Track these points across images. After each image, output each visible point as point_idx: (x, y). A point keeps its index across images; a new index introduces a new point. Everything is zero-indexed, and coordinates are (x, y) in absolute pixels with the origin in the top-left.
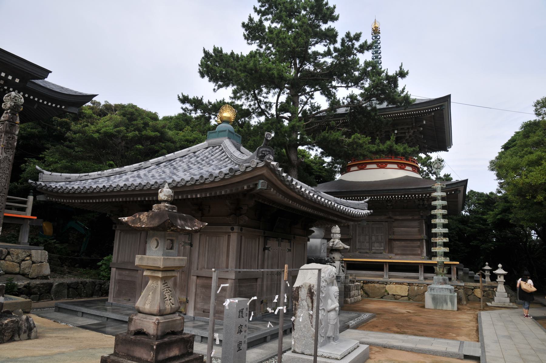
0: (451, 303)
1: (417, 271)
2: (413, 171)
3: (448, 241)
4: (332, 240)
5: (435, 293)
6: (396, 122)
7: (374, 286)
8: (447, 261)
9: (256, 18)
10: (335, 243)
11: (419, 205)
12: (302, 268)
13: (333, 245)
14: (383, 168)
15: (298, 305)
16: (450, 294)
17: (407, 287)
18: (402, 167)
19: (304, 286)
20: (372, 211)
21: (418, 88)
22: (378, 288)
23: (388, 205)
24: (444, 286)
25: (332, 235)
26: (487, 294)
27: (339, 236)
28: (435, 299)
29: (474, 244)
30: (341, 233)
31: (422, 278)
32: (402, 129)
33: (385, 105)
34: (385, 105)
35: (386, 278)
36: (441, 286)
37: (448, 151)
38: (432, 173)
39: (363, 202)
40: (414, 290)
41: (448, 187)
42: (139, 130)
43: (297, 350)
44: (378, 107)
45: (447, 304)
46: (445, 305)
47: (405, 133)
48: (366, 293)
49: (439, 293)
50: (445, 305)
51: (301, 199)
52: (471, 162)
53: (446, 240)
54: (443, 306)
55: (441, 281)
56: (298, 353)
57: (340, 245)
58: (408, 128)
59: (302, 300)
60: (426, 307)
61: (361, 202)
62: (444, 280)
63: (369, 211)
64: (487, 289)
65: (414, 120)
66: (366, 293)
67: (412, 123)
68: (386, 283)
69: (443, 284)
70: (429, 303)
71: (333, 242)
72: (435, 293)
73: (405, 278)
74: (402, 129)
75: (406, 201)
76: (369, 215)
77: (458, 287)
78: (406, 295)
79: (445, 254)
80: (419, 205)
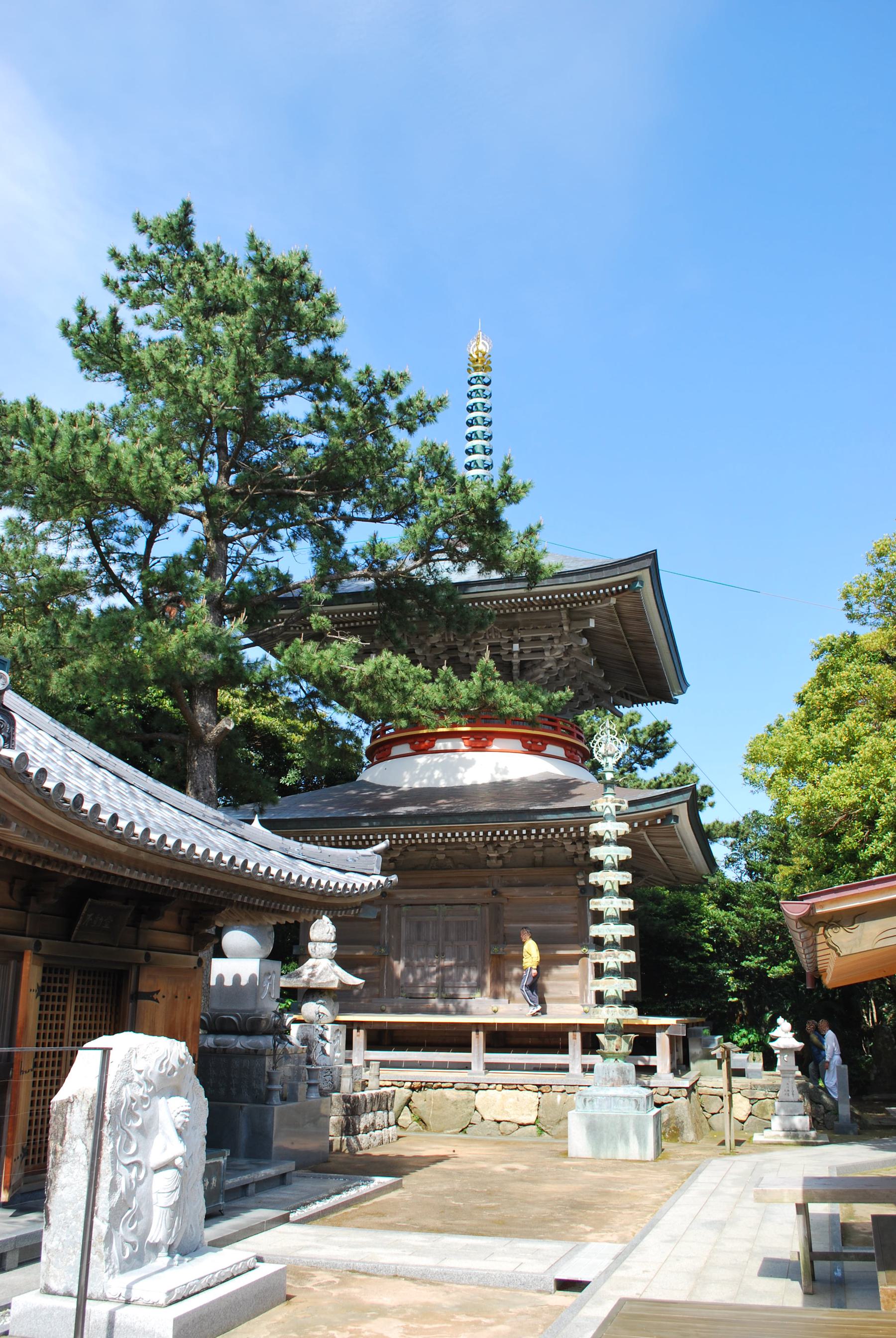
0: (639, 1139)
1: (466, 1047)
2: (570, 759)
3: (634, 960)
4: (310, 962)
5: (597, 1112)
6: (510, 619)
7: (443, 1095)
8: (631, 1014)
9: (102, 303)
10: (319, 970)
11: (576, 855)
12: (85, 1046)
13: (312, 975)
14: (482, 748)
15: (63, 1153)
16: (635, 1113)
17: (532, 1097)
18: (534, 746)
19: (80, 1098)
20: (394, 878)
21: (567, 532)
22: (455, 1103)
23: (489, 858)
24: (622, 1091)
25: (311, 946)
26: (759, 1107)
27: (330, 948)
28: (594, 1128)
29: (752, 964)
30: (339, 940)
31: (576, 1069)
32: (536, 640)
33: (472, 572)
34: (472, 572)
35: (477, 1073)
36: (613, 1091)
37: (675, 702)
38: (642, 763)
39: (368, 851)
40: (554, 1105)
41: (633, 809)
42: (267, 361)
43: (54, 1286)
44: (456, 578)
45: (627, 1142)
46: (621, 1145)
47: (542, 651)
48: (421, 1120)
49: (605, 1112)
50: (621, 1145)
51: (123, 849)
52: (727, 738)
53: (630, 957)
54: (616, 1148)
55: (615, 1075)
56: (55, 1294)
57: (333, 977)
58: (551, 639)
59: (74, 1139)
60: (572, 1153)
61: (362, 852)
62: (622, 1072)
63: (383, 879)
64: (760, 1094)
65: (564, 616)
66: (421, 1120)
67: (561, 626)
68: (477, 1088)
69: (618, 1085)
70: (578, 1142)
71: (314, 967)
72: (595, 1110)
73: (536, 1068)
74: (536, 640)
75: (540, 845)
76: (384, 893)
77: (672, 1091)
78: (532, 1119)
79: (628, 1000)
80: (576, 855)
